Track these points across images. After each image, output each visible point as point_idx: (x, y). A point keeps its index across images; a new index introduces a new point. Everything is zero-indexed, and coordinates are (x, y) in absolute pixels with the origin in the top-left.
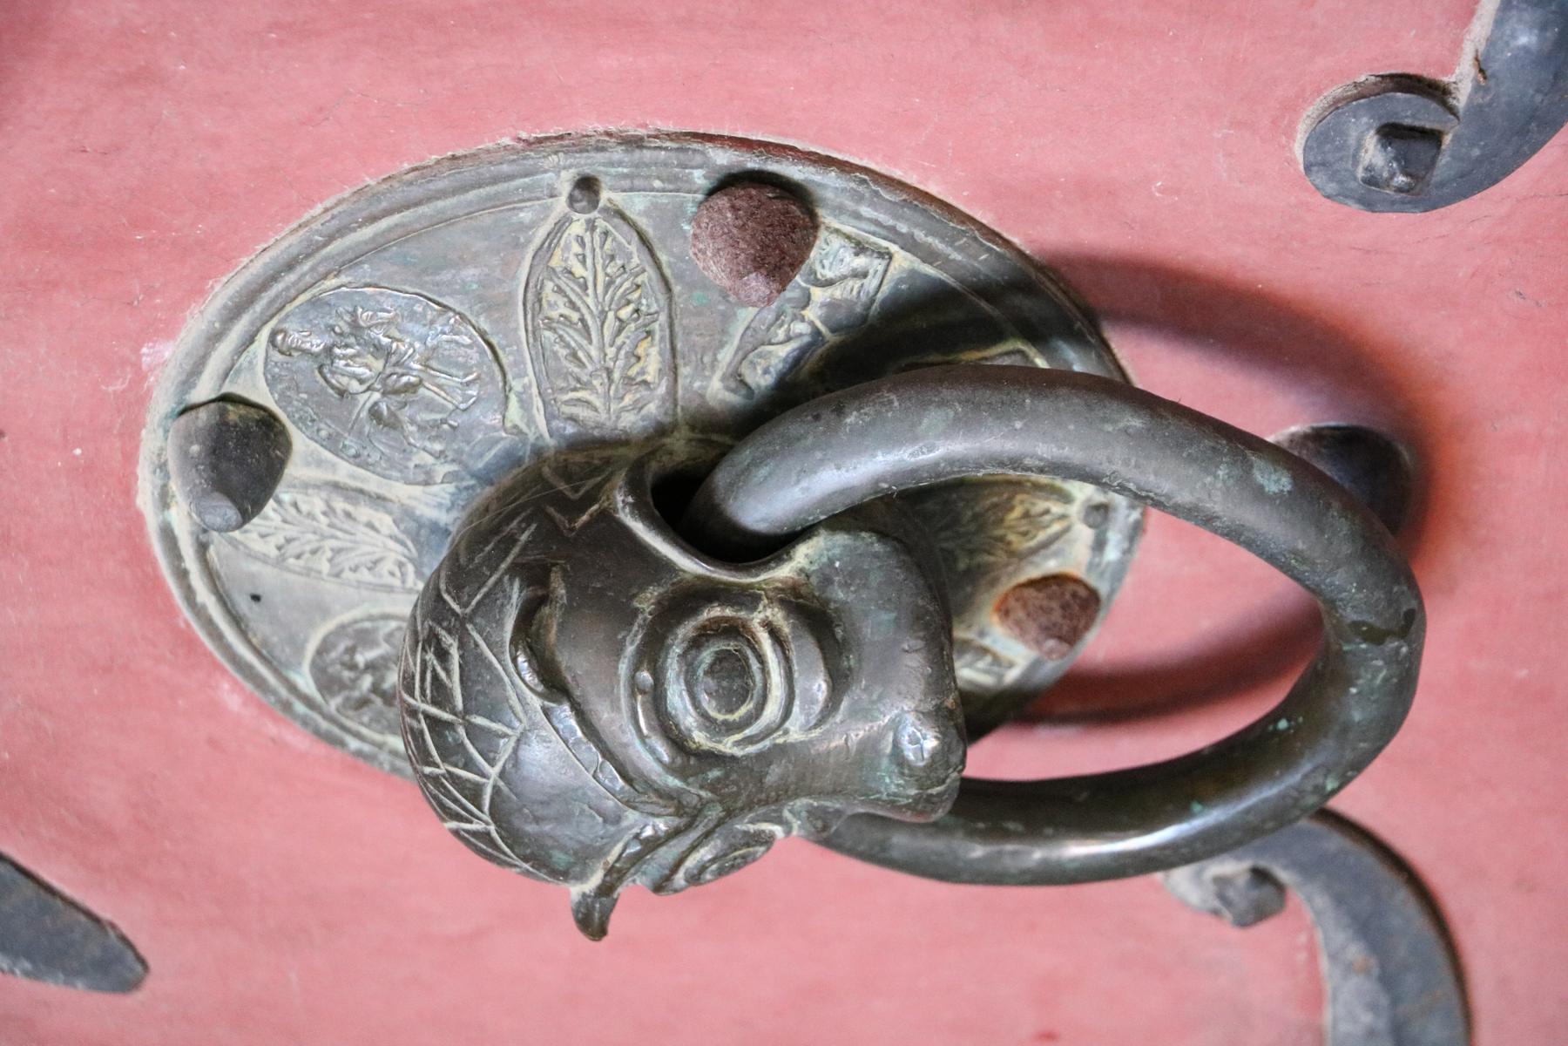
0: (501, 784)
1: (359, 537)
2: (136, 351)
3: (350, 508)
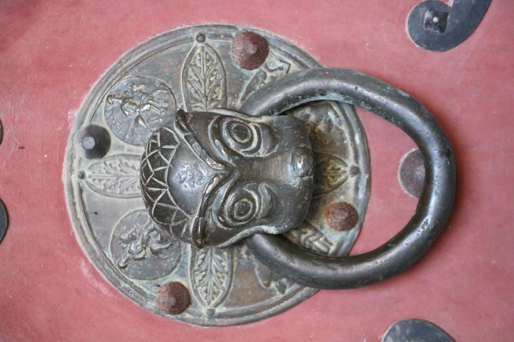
0: (171, 166)
1: (130, 174)
2: (66, 113)
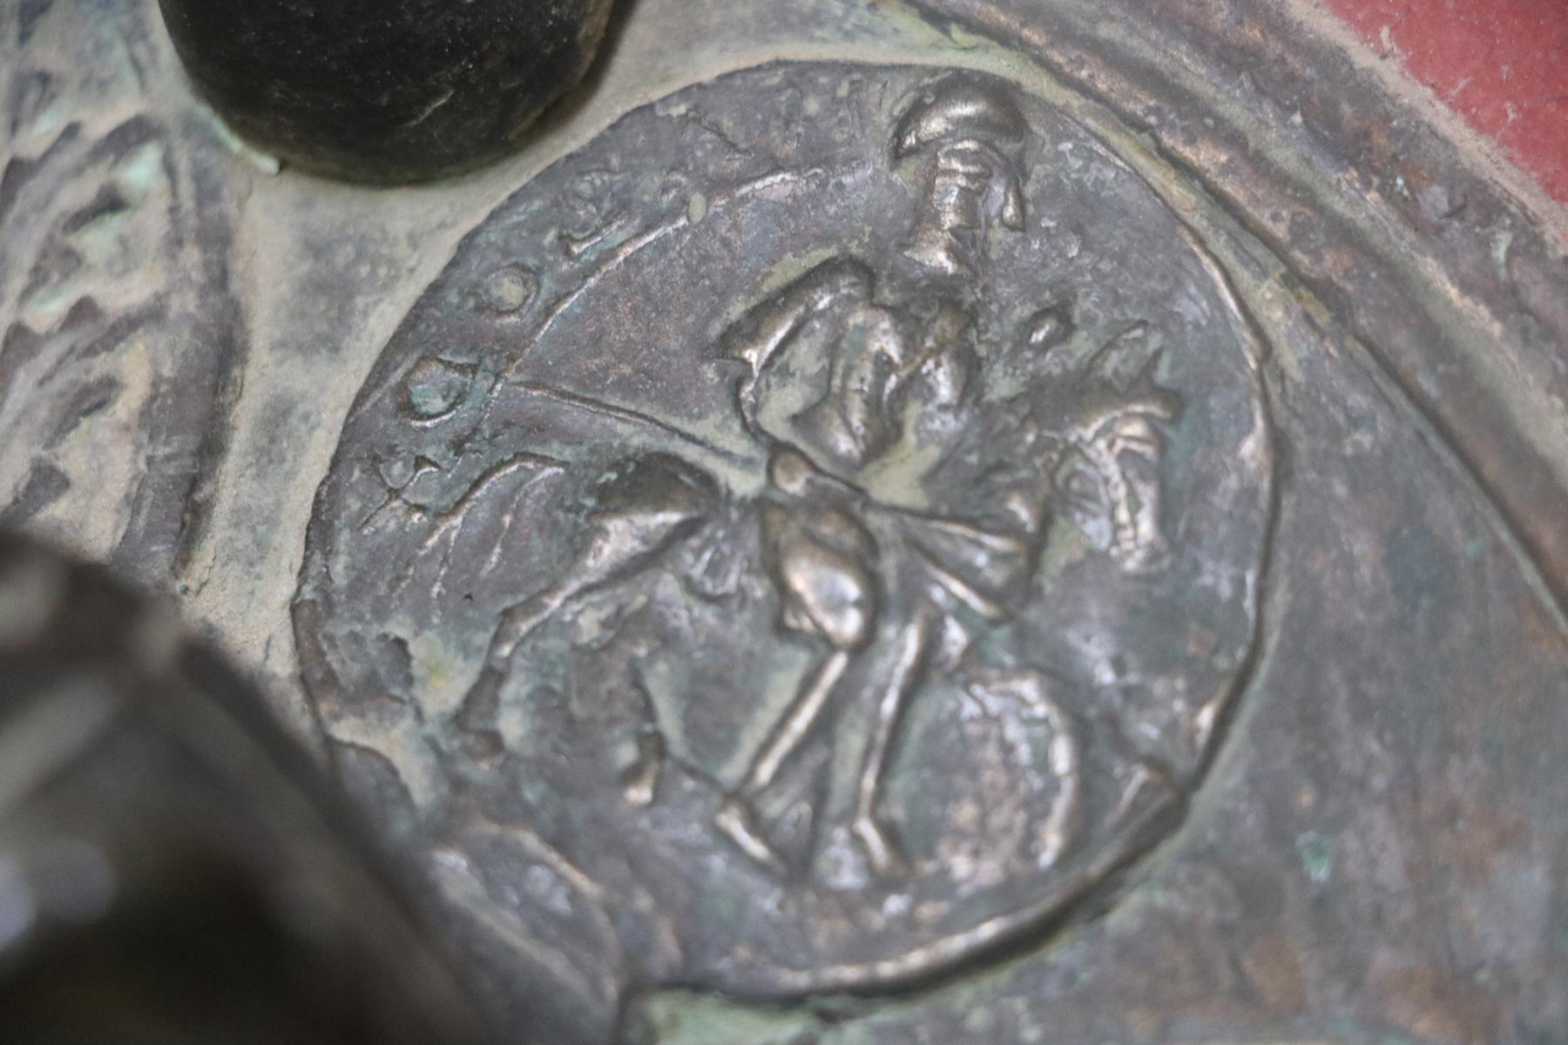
3: (126, 405)
